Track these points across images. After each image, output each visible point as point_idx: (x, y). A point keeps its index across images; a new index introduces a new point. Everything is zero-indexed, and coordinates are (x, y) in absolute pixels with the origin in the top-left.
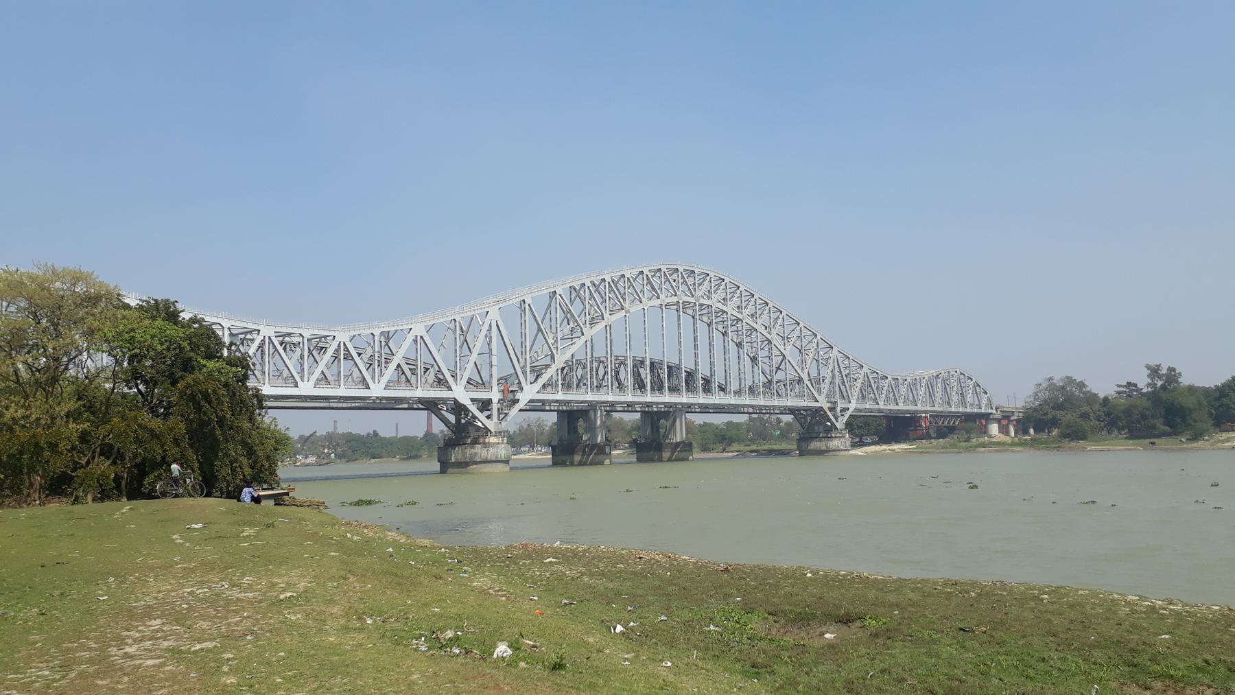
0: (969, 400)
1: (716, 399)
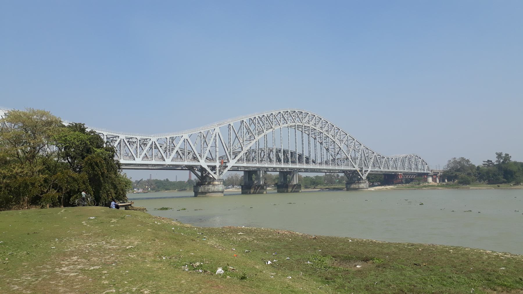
0: (419, 167)
1: (311, 166)
